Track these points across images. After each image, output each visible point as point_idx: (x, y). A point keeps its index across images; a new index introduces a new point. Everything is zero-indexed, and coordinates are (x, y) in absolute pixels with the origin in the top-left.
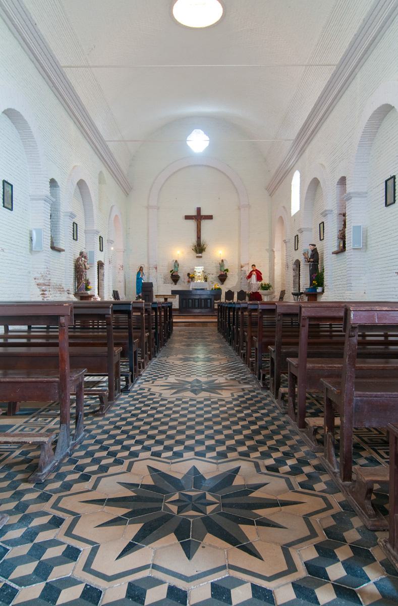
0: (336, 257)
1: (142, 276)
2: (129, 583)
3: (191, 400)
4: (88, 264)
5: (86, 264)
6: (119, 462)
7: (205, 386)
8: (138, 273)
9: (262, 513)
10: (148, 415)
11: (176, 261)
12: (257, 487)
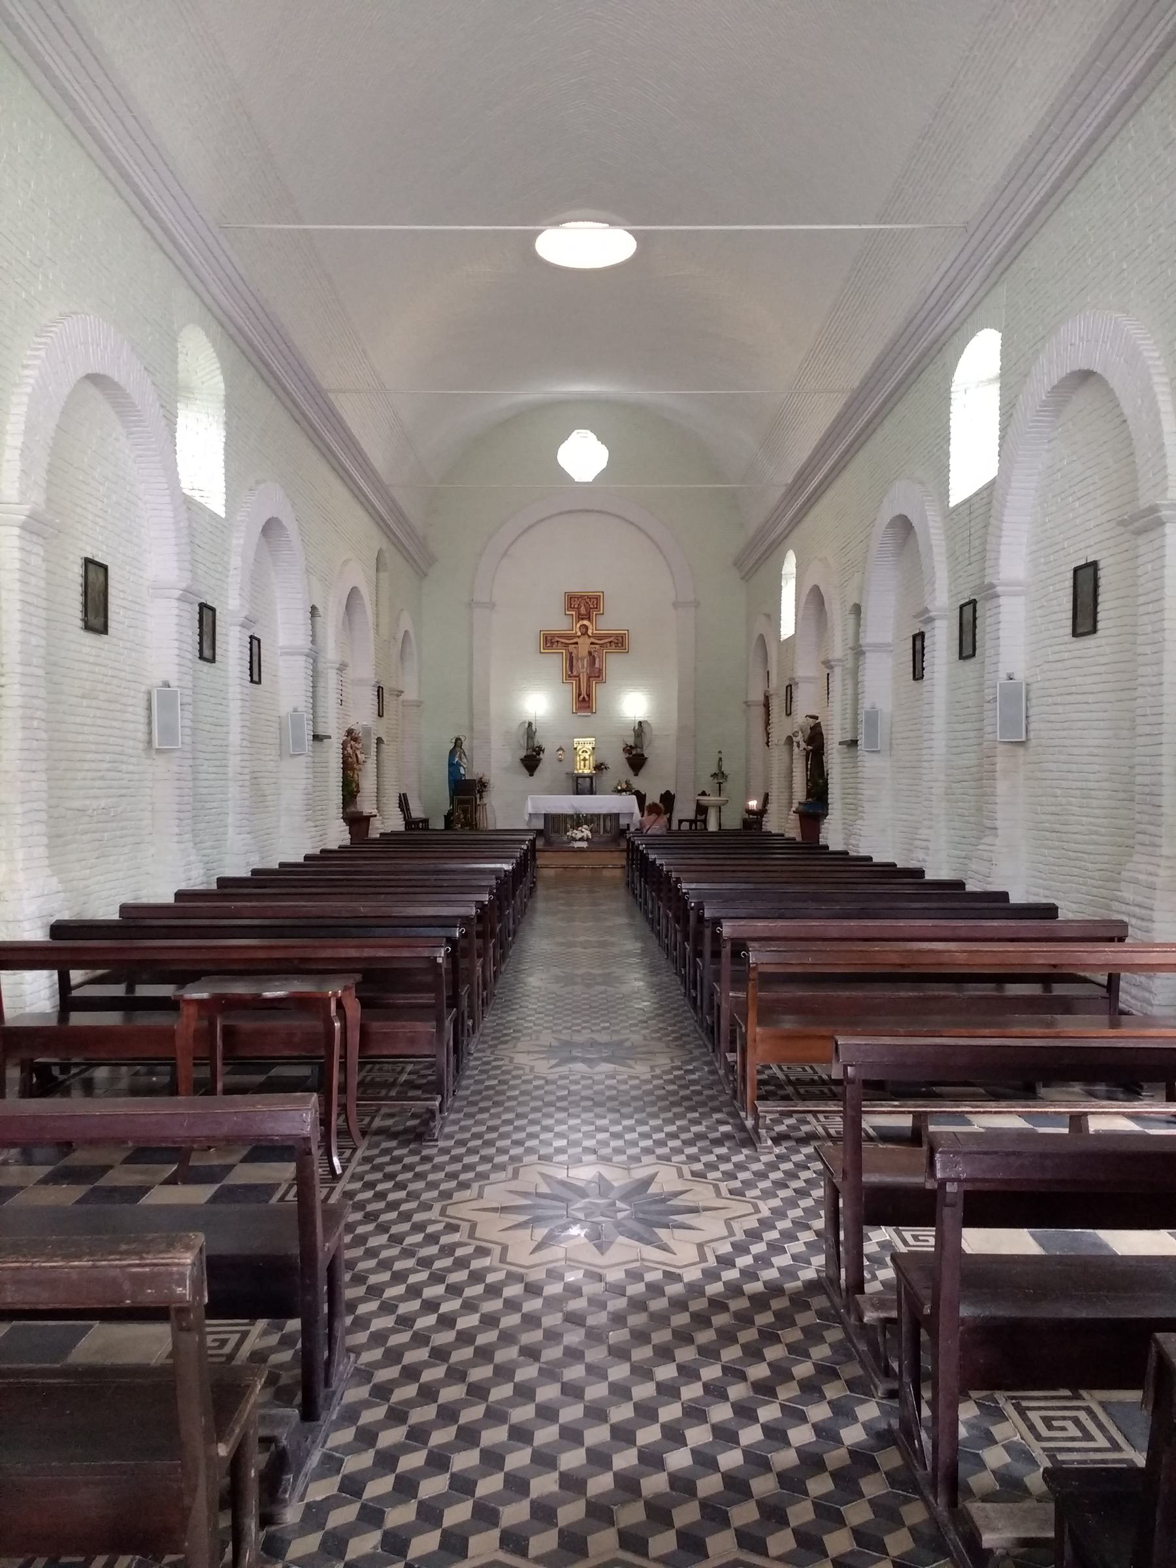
0: (846, 750)
1: (460, 758)
2: (466, 1557)
3: (583, 1078)
4: (362, 753)
5: (358, 752)
6: (502, 1167)
7: (599, 980)
8: (452, 753)
9: (678, 1218)
10: (404, 1166)
11: (530, 724)
12: (677, 1194)
